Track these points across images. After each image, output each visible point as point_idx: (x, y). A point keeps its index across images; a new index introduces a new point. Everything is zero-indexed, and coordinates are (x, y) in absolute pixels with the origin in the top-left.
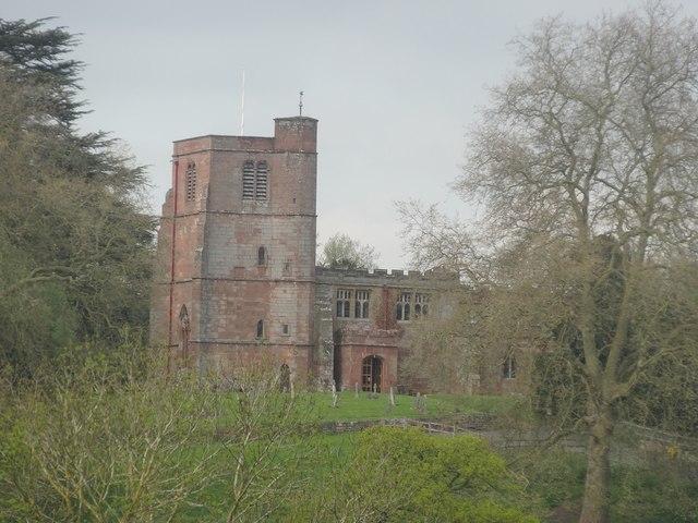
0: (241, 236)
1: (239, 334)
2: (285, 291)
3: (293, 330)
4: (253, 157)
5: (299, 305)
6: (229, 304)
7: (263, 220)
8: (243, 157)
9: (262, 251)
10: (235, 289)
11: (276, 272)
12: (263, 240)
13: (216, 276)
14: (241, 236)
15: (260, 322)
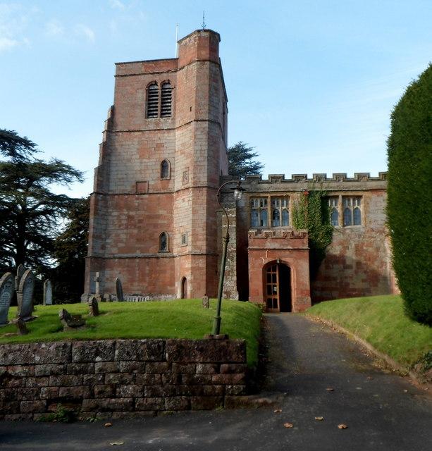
1: (139, 248)
2: (183, 200)
5: (194, 212)
6: (130, 218)
7: (166, 135)
9: (164, 165)
10: (136, 203)
11: (178, 184)
12: (165, 155)
15: (163, 235)
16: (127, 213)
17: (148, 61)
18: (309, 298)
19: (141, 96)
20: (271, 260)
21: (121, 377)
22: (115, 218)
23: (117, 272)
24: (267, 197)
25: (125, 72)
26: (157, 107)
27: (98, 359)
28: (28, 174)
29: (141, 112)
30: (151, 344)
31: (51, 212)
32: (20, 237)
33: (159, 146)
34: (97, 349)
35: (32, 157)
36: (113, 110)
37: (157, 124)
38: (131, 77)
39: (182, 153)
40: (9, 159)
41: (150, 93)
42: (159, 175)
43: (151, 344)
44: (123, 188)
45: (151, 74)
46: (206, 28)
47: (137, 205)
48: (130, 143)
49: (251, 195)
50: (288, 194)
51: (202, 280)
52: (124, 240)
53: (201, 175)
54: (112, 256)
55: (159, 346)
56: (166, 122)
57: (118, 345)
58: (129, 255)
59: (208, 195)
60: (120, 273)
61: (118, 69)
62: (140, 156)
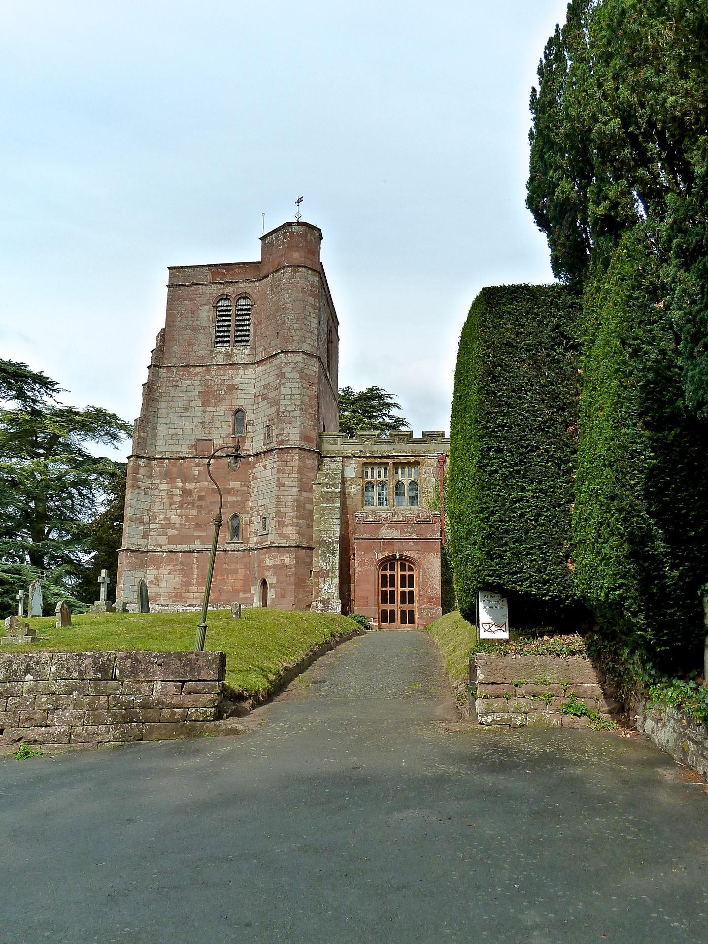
0: (208, 397)
1: (199, 537)
2: (265, 467)
3: (272, 524)
4: (230, 290)
6: (186, 492)
7: (241, 372)
8: (215, 290)
9: (239, 413)
13: (168, 455)
14: (208, 397)
16: (180, 485)
17: (216, 265)
18: (440, 609)
19: (206, 314)
20: (387, 554)
21: (57, 700)
22: (165, 493)
23: (166, 572)
24: (388, 464)
25: (182, 280)
26: (229, 331)
27: (29, 677)
28: (36, 432)
29: (204, 340)
30: (99, 658)
31: (86, 483)
32: (35, 521)
33: (232, 388)
34: (28, 665)
35: (49, 401)
36: (163, 336)
37: (229, 356)
38: (192, 288)
39: (264, 399)
40: (13, 406)
41: (222, 315)
42: (230, 430)
43: (99, 658)
44: (177, 448)
45: (221, 283)
46: (301, 220)
47: (196, 473)
48: (188, 383)
49: (365, 460)
50: (417, 459)
51: (289, 584)
52: (177, 526)
53: (291, 431)
54: (158, 549)
55: (108, 660)
56: (241, 353)
57: (55, 659)
58: (185, 547)
59: (301, 459)
60: (169, 573)
61: (172, 276)
62: (203, 403)
